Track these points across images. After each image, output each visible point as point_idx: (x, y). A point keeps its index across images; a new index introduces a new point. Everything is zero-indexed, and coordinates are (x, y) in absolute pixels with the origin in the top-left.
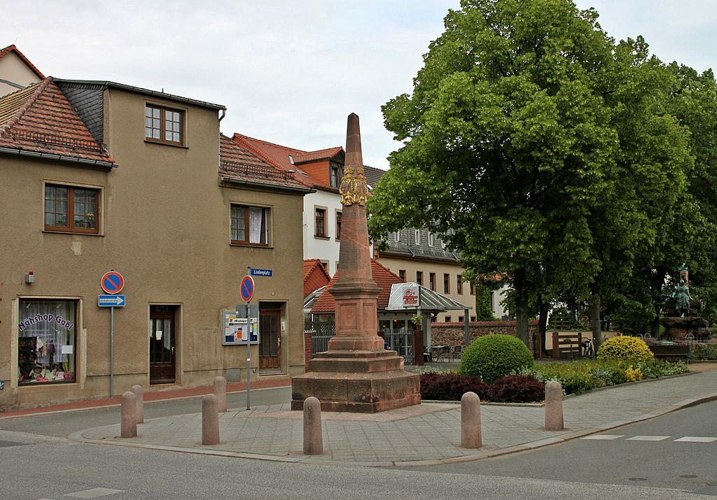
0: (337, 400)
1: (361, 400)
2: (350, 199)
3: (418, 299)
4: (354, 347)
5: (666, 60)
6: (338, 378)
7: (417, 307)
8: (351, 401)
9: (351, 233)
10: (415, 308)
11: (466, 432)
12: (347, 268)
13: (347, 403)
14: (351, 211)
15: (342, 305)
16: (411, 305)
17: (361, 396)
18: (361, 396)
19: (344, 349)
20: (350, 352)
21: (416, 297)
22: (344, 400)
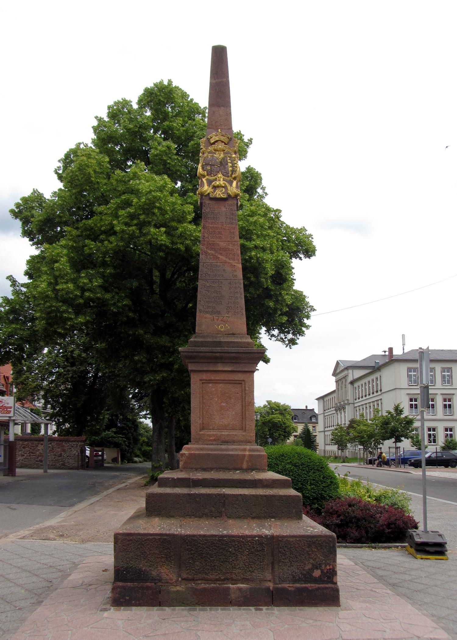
0: (245, 580)
1: (308, 578)
2: (225, 187)
3: (12, 410)
4: (245, 466)
5: (314, 244)
6: (247, 533)
7: (10, 417)
8: (282, 581)
9: (225, 249)
10: (8, 418)
11: (83, 541)
12: (219, 313)
13: (271, 585)
14: (224, 209)
15: (209, 381)
16: (4, 415)
17: (312, 570)
18: (312, 570)
19: (204, 470)
20: (237, 475)
21: (11, 408)
22: (262, 580)
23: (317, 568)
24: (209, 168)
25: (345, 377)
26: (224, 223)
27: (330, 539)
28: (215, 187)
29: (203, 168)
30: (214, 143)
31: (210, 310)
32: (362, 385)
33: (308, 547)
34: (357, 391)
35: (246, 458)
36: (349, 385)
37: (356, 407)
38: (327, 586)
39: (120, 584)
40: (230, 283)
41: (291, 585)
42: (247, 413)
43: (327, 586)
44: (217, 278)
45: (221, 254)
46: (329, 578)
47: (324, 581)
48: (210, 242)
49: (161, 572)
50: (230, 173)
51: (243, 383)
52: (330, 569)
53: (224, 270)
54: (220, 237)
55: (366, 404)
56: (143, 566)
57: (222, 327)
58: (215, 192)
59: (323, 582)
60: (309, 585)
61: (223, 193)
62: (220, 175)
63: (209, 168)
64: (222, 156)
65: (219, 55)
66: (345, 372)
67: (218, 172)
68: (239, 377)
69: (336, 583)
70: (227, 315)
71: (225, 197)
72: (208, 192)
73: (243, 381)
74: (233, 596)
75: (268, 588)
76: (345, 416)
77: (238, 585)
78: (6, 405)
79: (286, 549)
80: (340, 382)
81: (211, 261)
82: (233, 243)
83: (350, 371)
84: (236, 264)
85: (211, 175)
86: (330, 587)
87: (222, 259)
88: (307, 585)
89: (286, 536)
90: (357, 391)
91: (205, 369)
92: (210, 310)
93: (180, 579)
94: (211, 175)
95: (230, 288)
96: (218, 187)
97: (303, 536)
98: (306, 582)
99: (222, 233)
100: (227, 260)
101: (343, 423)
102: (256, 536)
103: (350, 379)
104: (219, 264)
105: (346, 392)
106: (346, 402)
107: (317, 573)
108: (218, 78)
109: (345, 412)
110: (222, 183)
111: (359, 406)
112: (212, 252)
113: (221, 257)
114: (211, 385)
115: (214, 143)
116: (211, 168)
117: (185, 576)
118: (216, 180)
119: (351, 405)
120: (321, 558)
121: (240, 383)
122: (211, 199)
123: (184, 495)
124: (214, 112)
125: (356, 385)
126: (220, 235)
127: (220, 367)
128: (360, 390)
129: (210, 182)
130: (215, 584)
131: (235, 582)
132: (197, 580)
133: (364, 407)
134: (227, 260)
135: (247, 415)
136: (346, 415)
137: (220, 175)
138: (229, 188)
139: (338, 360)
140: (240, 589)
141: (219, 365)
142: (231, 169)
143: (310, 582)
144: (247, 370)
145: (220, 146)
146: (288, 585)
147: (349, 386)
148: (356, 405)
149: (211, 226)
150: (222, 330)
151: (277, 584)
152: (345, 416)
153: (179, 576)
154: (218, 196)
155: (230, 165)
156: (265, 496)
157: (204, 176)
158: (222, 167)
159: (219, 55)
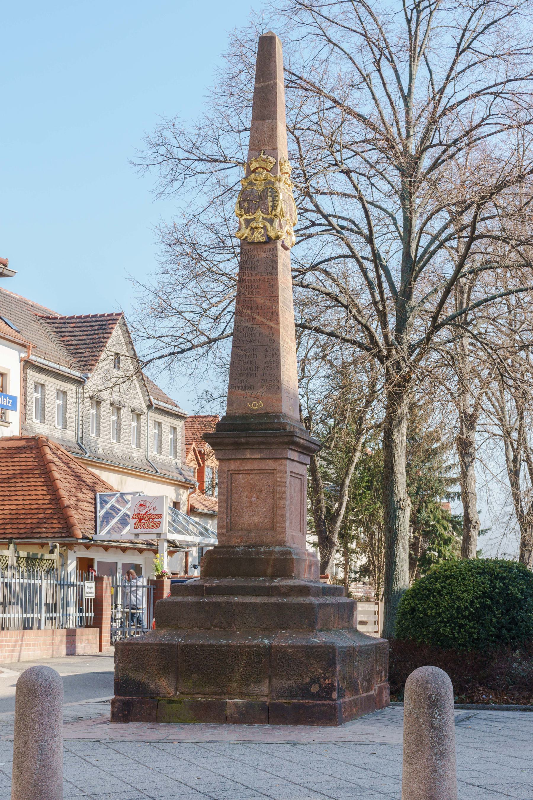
0: (242, 695)
1: (306, 693)
2: (265, 228)
12: (252, 387)
13: (267, 700)
17: (310, 684)
18: (310, 684)
23: (315, 682)
26: (263, 274)
27: (330, 650)
28: (252, 229)
31: (243, 384)
33: (307, 659)
35: (271, 562)
38: (325, 702)
39: (119, 697)
40: (266, 350)
41: (288, 701)
42: (278, 508)
43: (325, 702)
44: (252, 344)
45: (258, 314)
46: (327, 693)
47: (322, 697)
48: (247, 299)
49: (159, 686)
50: (270, 209)
51: (275, 472)
52: (329, 684)
53: (260, 334)
54: (257, 293)
56: (143, 677)
57: (255, 405)
58: (253, 234)
59: (322, 698)
60: (307, 701)
61: (262, 236)
67: (257, 209)
68: (270, 465)
70: (261, 390)
72: (246, 235)
73: (275, 470)
74: (229, 712)
75: (264, 704)
77: (235, 700)
78: (152, 512)
79: (284, 661)
81: (246, 323)
82: (273, 298)
84: (273, 326)
85: (248, 213)
86: (327, 704)
87: (258, 320)
88: (304, 701)
91: (232, 457)
92: (243, 384)
93: (178, 693)
94: (248, 213)
95: (266, 356)
98: (304, 698)
99: (261, 286)
100: (264, 321)
102: (253, 646)
104: (254, 326)
107: (315, 689)
108: (263, 82)
112: (248, 312)
113: (257, 317)
114: (240, 476)
116: (249, 205)
120: (320, 671)
121: (272, 472)
124: (257, 128)
126: (257, 290)
130: (212, 698)
131: (231, 695)
132: (194, 694)
134: (264, 321)
135: (278, 511)
140: (236, 704)
141: (248, 451)
143: (307, 698)
144: (278, 457)
146: (285, 701)
149: (248, 278)
150: (255, 408)
151: (274, 699)
153: (176, 689)
155: (270, 199)
158: (261, 202)
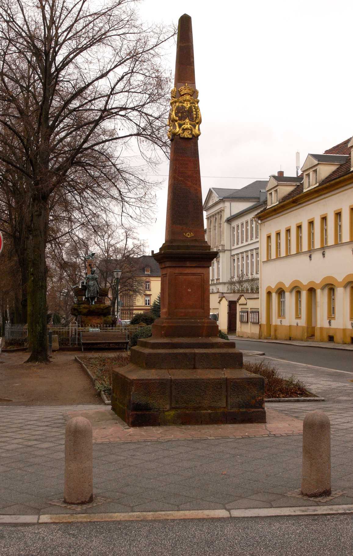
20: (201, 340)
24: (180, 115)
25: (220, 212)
28: (184, 130)
29: (176, 115)
30: (183, 95)
32: (242, 224)
34: (235, 233)
36: (225, 223)
37: (234, 255)
50: (195, 119)
55: (247, 252)
57: (188, 235)
62: (187, 121)
63: (180, 115)
64: (189, 105)
65: (185, 23)
66: (221, 206)
69: (264, 408)
71: (191, 137)
76: (218, 268)
80: (213, 220)
83: (227, 204)
89: (235, 379)
90: (235, 233)
96: (186, 129)
97: (244, 379)
101: (216, 277)
103: (226, 215)
105: (221, 234)
106: (220, 248)
109: (218, 262)
110: (189, 126)
111: (237, 254)
115: (183, 95)
117: (173, 405)
118: (184, 124)
119: (227, 253)
122: (181, 138)
123: (166, 354)
125: (234, 224)
127: (188, 264)
128: (240, 231)
129: (180, 126)
133: (245, 255)
136: (220, 266)
137: (187, 121)
138: (193, 130)
139: (211, 187)
142: (195, 116)
145: (188, 97)
147: (225, 226)
148: (234, 253)
152: (218, 268)
154: (186, 136)
155: (194, 113)
156: (220, 353)
157: (176, 121)
159: (185, 23)
